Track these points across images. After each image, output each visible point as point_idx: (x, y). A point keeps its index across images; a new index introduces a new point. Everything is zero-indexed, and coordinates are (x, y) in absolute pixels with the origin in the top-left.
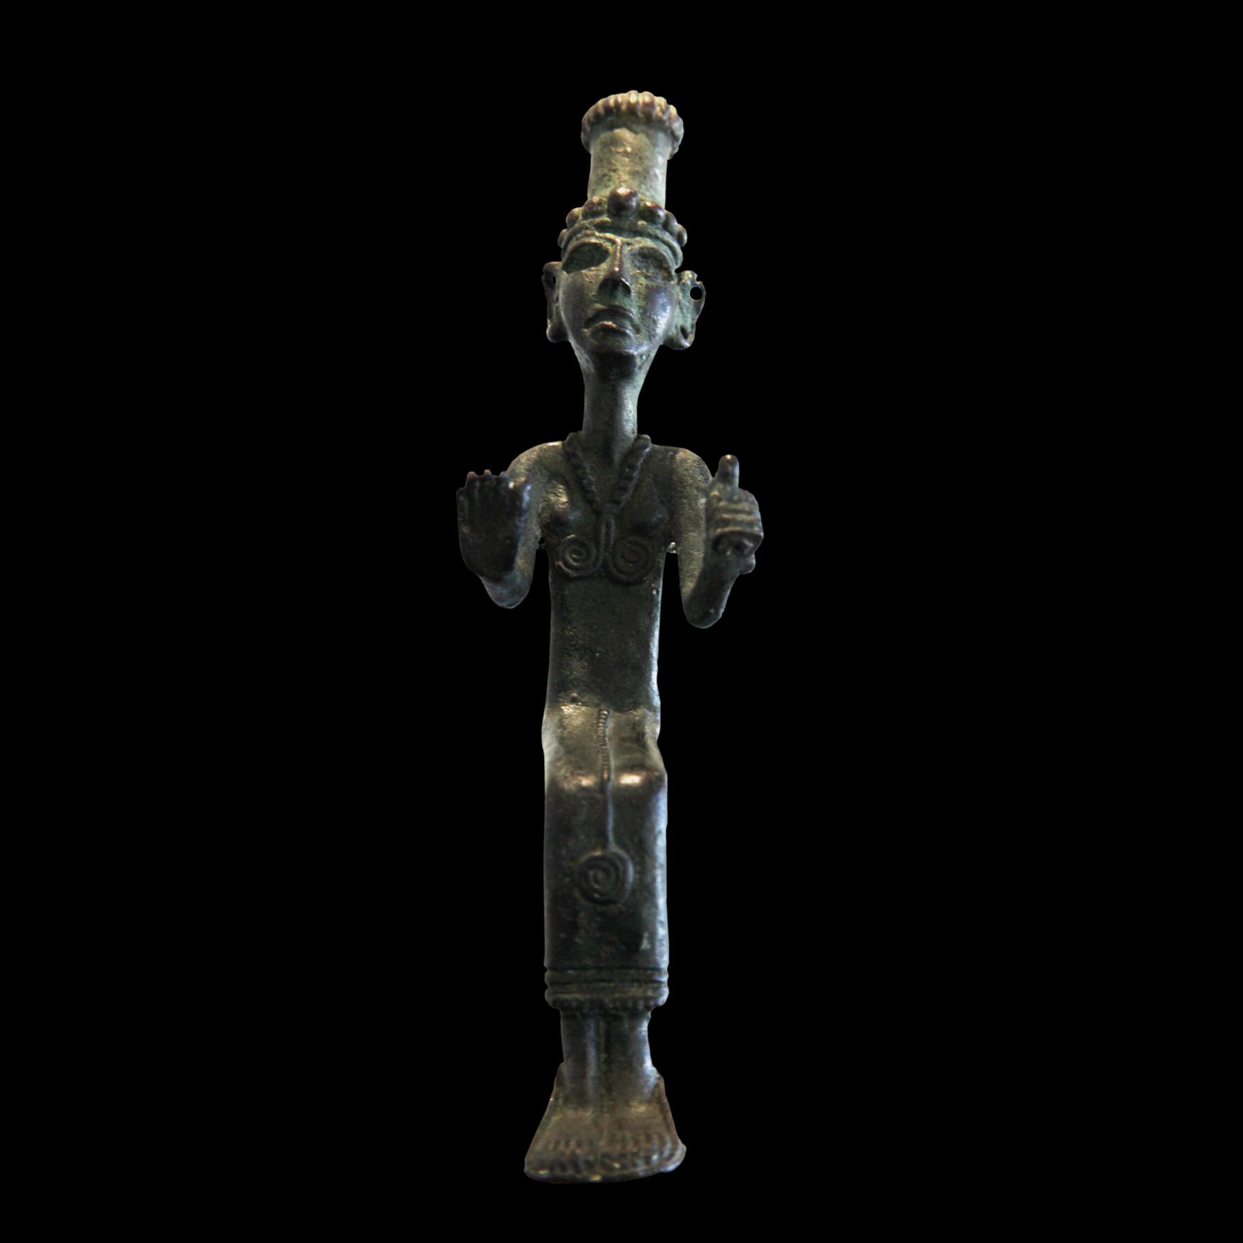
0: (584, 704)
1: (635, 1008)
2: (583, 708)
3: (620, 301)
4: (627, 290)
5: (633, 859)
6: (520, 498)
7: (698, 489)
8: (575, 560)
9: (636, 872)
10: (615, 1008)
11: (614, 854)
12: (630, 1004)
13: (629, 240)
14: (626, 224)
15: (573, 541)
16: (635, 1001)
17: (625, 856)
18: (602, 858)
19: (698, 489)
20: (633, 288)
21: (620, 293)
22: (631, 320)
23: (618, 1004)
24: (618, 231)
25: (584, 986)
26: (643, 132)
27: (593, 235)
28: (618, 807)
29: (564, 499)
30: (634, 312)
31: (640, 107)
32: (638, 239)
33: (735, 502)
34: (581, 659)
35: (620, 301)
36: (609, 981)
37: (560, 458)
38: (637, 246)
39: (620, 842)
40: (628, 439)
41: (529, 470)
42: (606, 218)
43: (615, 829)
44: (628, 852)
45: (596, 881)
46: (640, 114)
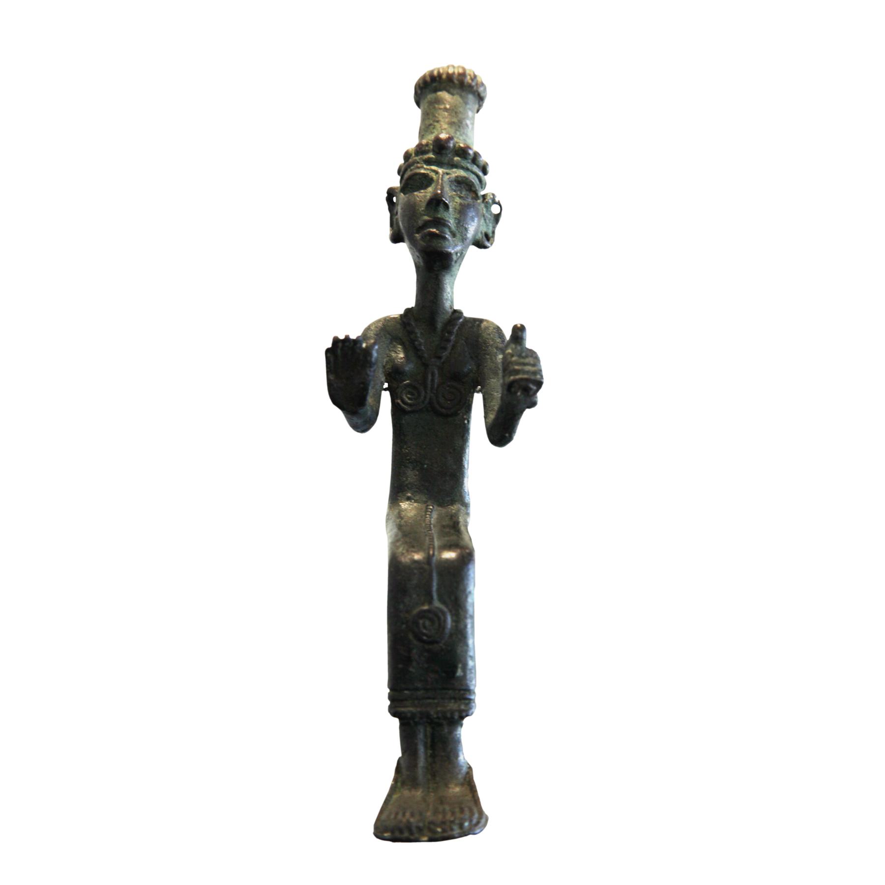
0: (416, 501)
1: (452, 718)
2: (415, 504)
3: (442, 214)
4: (446, 207)
5: (451, 611)
6: (370, 355)
7: (497, 348)
8: (409, 399)
9: (453, 621)
10: (438, 718)
11: (437, 608)
12: (449, 715)
13: (448, 171)
14: (446, 160)
15: (408, 385)
16: (452, 712)
17: (445, 609)
18: (428, 611)
19: (497, 348)
20: (451, 205)
21: (441, 209)
22: (449, 228)
23: (440, 715)
24: (440, 164)
25: (416, 702)
26: (458, 94)
27: (422, 167)
28: (440, 574)
29: (402, 355)
30: (452, 222)
31: (455, 76)
32: (454, 170)
33: (523, 358)
34: (413, 469)
35: (442, 214)
36: (434, 699)
37: (399, 326)
38: (454, 175)
39: (441, 600)
40: (447, 312)
41: (377, 335)
42: (431, 155)
43: (438, 590)
44: (447, 606)
45: (425, 627)
46: (456, 81)
